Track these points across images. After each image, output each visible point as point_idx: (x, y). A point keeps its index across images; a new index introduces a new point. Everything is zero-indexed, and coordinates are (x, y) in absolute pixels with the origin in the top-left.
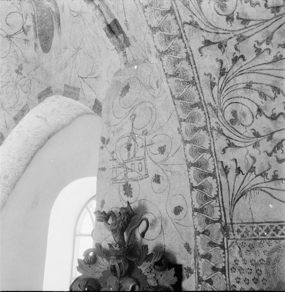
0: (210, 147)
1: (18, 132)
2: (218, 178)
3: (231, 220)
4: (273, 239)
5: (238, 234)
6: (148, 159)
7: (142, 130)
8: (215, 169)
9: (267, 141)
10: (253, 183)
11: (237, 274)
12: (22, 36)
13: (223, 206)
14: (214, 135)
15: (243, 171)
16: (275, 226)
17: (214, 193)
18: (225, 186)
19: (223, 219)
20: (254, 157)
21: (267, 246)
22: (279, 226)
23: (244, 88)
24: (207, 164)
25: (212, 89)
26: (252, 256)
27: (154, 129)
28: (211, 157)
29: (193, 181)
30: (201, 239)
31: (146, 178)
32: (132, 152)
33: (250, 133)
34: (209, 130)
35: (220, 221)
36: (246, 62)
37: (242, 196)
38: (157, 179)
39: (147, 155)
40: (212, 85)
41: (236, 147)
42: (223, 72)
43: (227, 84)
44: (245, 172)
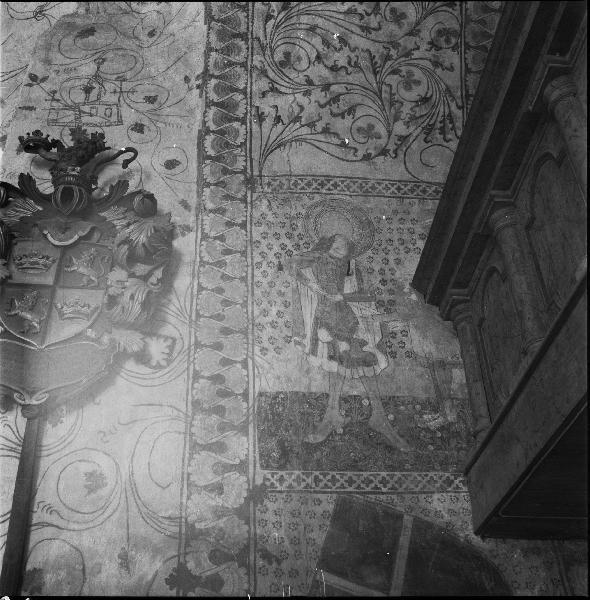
0: (246, 88)
3: (260, 172)
7: (116, 76)
8: (246, 113)
10: (295, 134)
11: (262, 229)
13: (251, 157)
17: (240, 140)
18: (256, 134)
19: (249, 171)
21: (307, 200)
24: (236, 106)
25: (266, 22)
26: (287, 209)
30: (211, 191)
33: (301, 79)
35: (244, 172)
37: (279, 146)
41: (281, 93)
44: (286, 121)
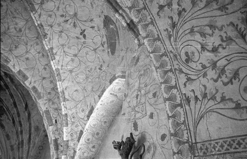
1: (101, 105)
2: (184, 107)
3: (195, 140)
4: (229, 153)
5: (201, 152)
6: (147, 102)
9: (212, 70)
12: (101, 48)
14: (177, 74)
15: (199, 98)
16: (238, 140)
17: (182, 119)
20: (205, 85)
22: (241, 139)
23: (189, 33)
27: (151, 82)
28: (177, 91)
29: (169, 112)
31: (146, 116)
32: (139, 99)
34: (174, 71)
35: (188, 142)
36: (188, 11)
38: (151, 116)
39: (146, 100)
40: (170, 37)
42: (174, 25)
43: (179, 33)
44: (201, 98)
